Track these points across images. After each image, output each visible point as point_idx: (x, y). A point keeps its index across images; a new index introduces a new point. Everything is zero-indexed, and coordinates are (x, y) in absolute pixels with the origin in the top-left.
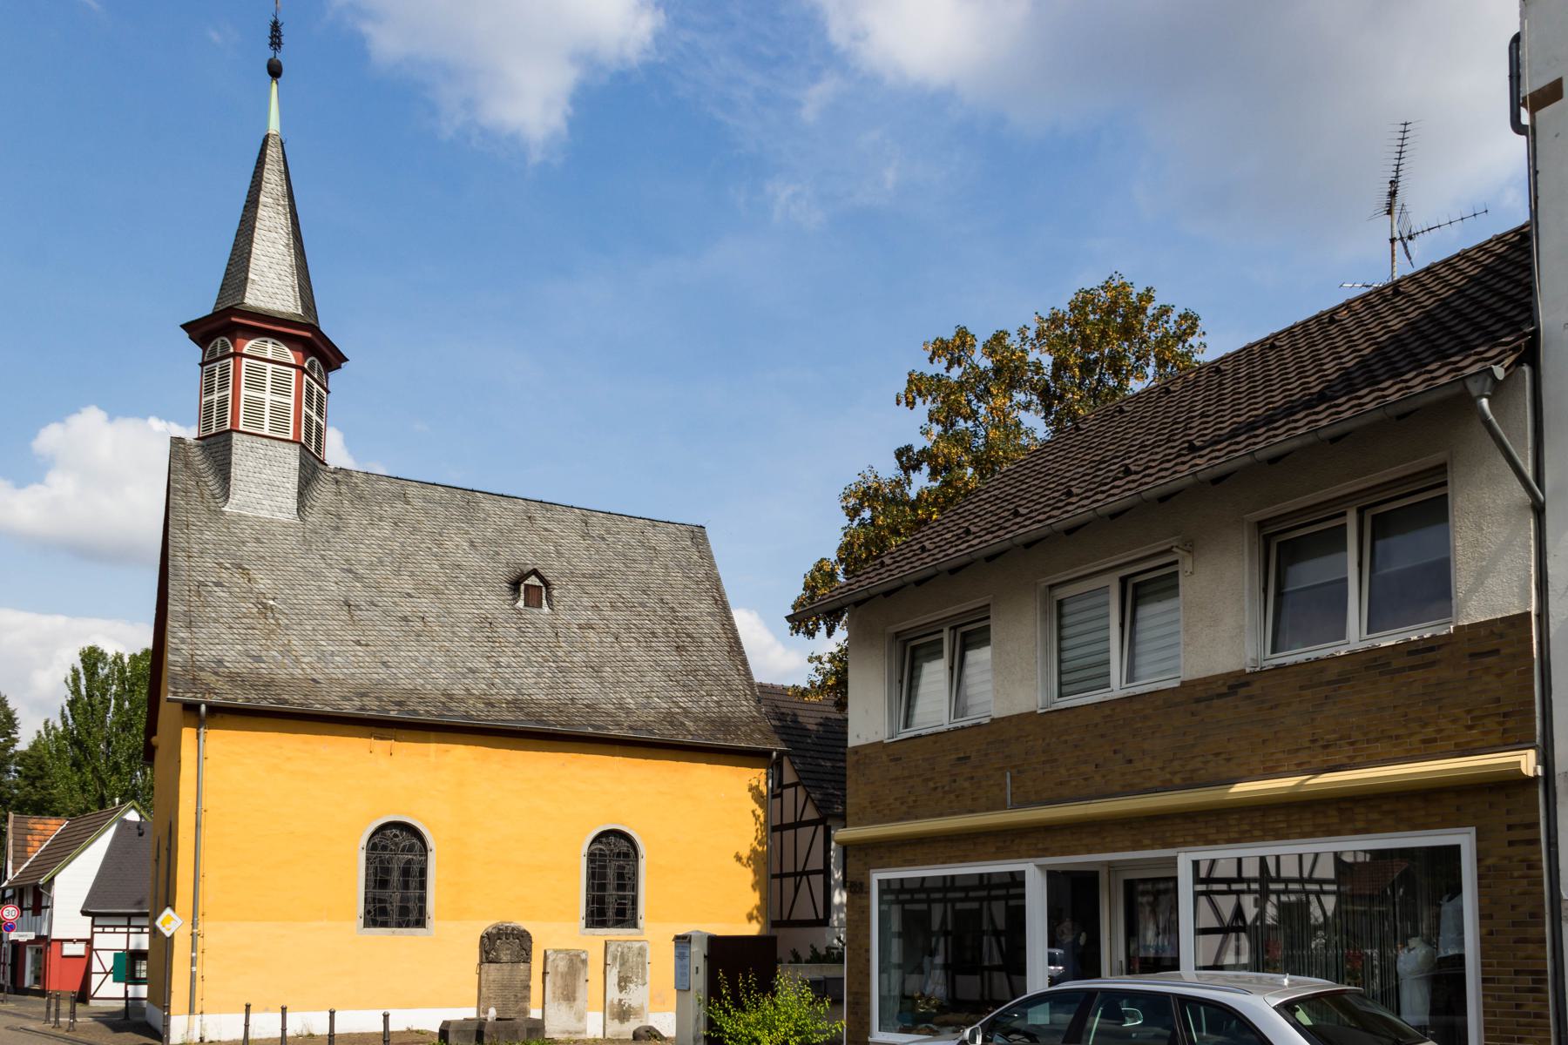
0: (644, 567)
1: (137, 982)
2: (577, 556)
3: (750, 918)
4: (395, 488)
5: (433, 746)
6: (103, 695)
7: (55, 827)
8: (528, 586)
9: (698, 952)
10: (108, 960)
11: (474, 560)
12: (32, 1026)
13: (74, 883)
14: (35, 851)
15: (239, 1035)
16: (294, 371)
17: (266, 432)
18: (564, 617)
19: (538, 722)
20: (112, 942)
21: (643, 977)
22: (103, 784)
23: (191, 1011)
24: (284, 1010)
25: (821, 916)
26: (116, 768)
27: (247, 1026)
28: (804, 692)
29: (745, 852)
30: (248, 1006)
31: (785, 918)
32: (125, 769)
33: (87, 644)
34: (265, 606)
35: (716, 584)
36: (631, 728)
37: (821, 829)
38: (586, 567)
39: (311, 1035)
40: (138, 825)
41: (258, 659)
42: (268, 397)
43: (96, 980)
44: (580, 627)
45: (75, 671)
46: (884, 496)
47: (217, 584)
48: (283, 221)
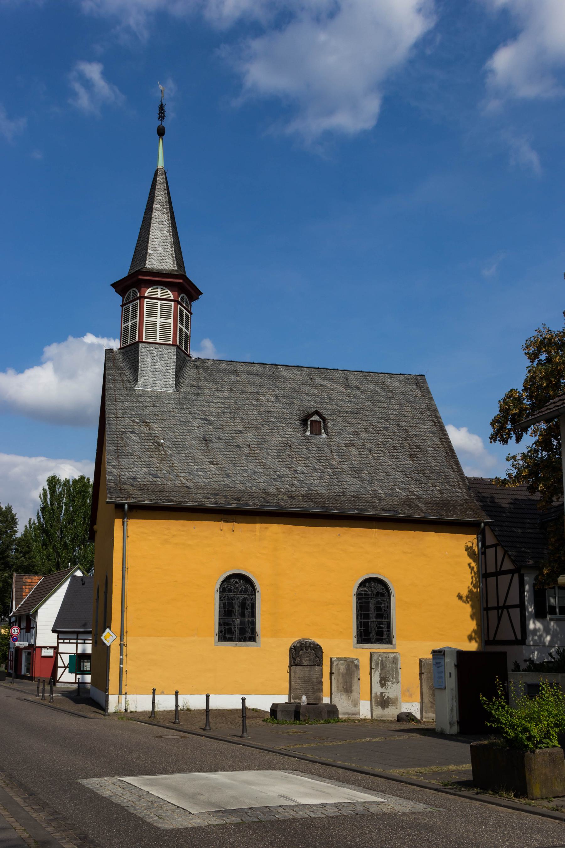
0: (386, 405)
1: (83, 673)
2: (342, 400)
3: (470, 638)
4: (230, 367)
5: (258, 526)
6: (59, 504)
7: (37, 580)
8: (313, 421)
9: (450, 662)
10: (66, 659)
11: (278, 408)
12: (30, 698)
13: (48, 613)
14: (27, 593)
15: (172, 707)
16: (173, 303)
17: (158, 341)
18: (336, 439)
19: (323, 507)
20: (68, 648)
21: (397, 678)
22: (59, 556)
23: (120, 693)
24: (177, 694)
25: (519, 638)
26: (65, 546)
27: (153, 702)
28: (504, 482)
29: (465, 593)
30: (154, 690)
31: (491, 638)
32: (70, 546)
33: (50, 474)
34: (159, 444)
35: (435, 412)
36: (383, 509)
37: (516, 576)
38: (349, 407)
39: (188, 710)
40: (82, 579)
41: (155, 476)
42: (158, 320)
43: (60, 671)
44: (346, 445)
45: (44, 490)
46: (556, 344)
47: (132, 433)
48: (166, 217)
